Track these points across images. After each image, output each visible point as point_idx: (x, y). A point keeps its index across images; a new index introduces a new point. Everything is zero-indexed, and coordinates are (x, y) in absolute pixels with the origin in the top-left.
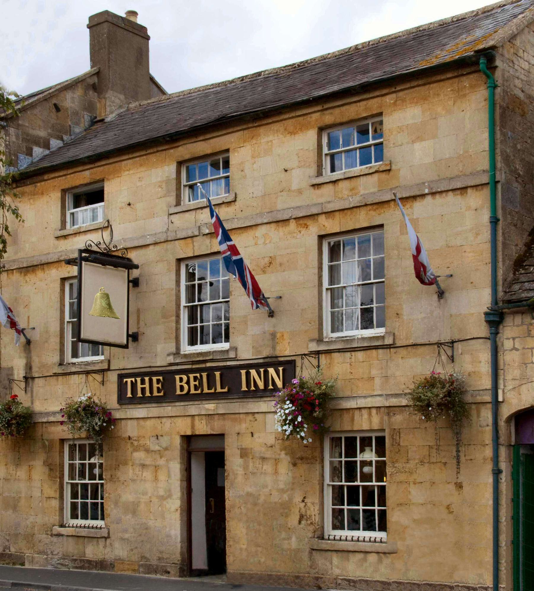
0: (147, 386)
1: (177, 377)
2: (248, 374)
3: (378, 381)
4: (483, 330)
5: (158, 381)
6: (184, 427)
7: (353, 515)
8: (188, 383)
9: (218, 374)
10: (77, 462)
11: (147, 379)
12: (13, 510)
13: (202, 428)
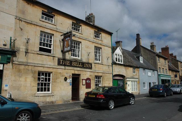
0: (66, 62)
1: (73, 62)
2: (86, 64)
3: (102, 69)
4: (111, 65)
5: (69, 62)
6: (73, 72)
7: (42, 88)
8: (75, 64)
9: (81, 63)
10: (99, 80)
11: (66, 61)
12: (18, 90)
13: (77, 73)
